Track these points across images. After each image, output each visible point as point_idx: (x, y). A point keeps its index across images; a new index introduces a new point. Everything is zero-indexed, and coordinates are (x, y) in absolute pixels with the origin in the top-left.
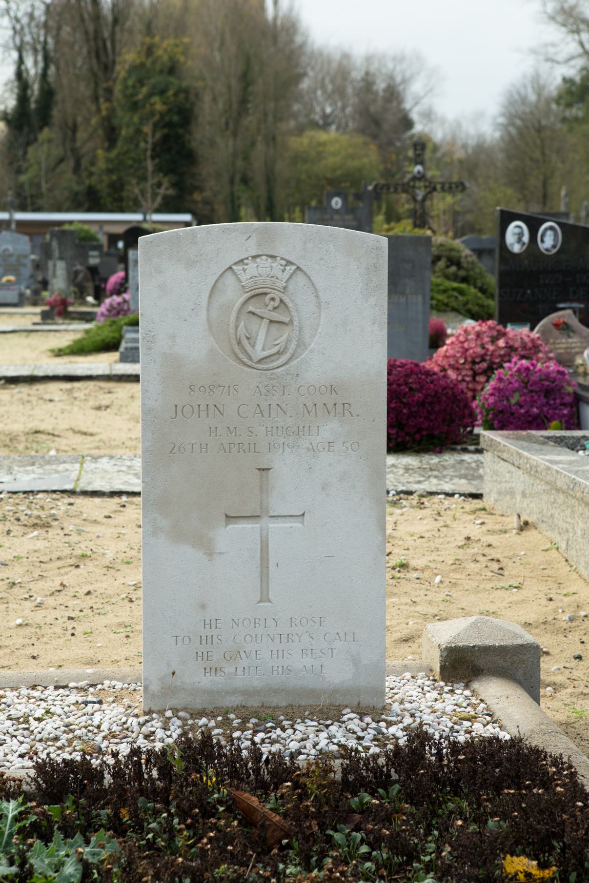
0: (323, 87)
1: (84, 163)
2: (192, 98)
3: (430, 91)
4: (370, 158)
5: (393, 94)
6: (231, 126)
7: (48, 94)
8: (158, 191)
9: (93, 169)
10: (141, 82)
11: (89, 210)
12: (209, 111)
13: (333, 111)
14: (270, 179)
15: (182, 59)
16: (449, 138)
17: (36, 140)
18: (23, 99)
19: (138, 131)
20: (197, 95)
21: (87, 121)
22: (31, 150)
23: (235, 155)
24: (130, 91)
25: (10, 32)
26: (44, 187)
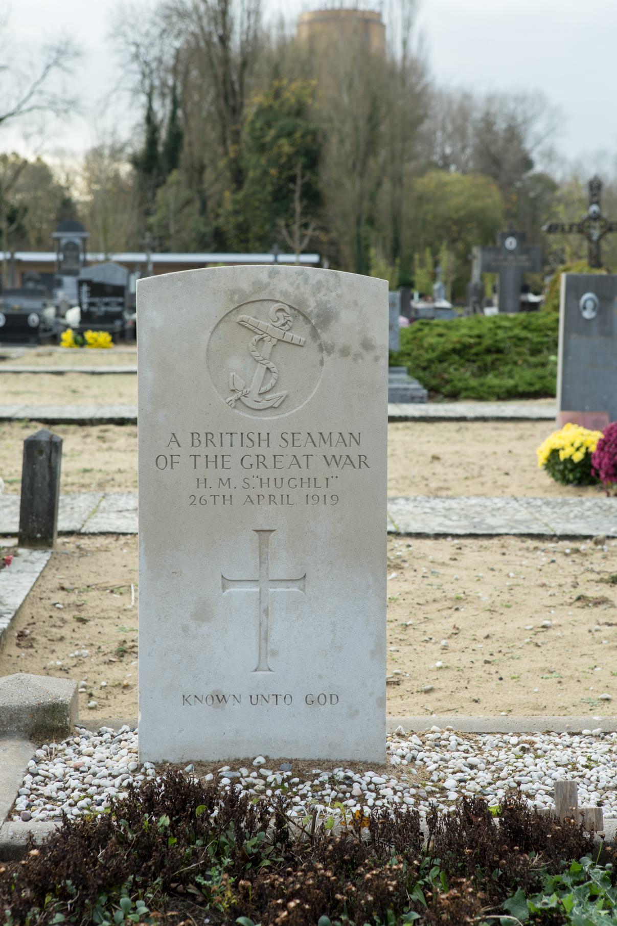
0: (444, 129)
1: (211, 204)
2: (320, 139)
3: (551, 130)
4: (492, 199)
5: (514, 135)
6: (358, 168)
7: (176, 137)
8: (305, 232)
9: (221, 211)
10: (269, 125)
11: (216, 251)
12: (336, 152)
13: (452, 153)
14: (396, 219)
15: (309, 101)
16: (569, 178)
17: (164, 182)
18: (152, 142)
19: (265, 173)
20: (324, 137)
21: (213, 161)
22: (160, 193)
23: (361, 197)
24: (258, 133)
25: (139, 77)
26: (173, 229)
